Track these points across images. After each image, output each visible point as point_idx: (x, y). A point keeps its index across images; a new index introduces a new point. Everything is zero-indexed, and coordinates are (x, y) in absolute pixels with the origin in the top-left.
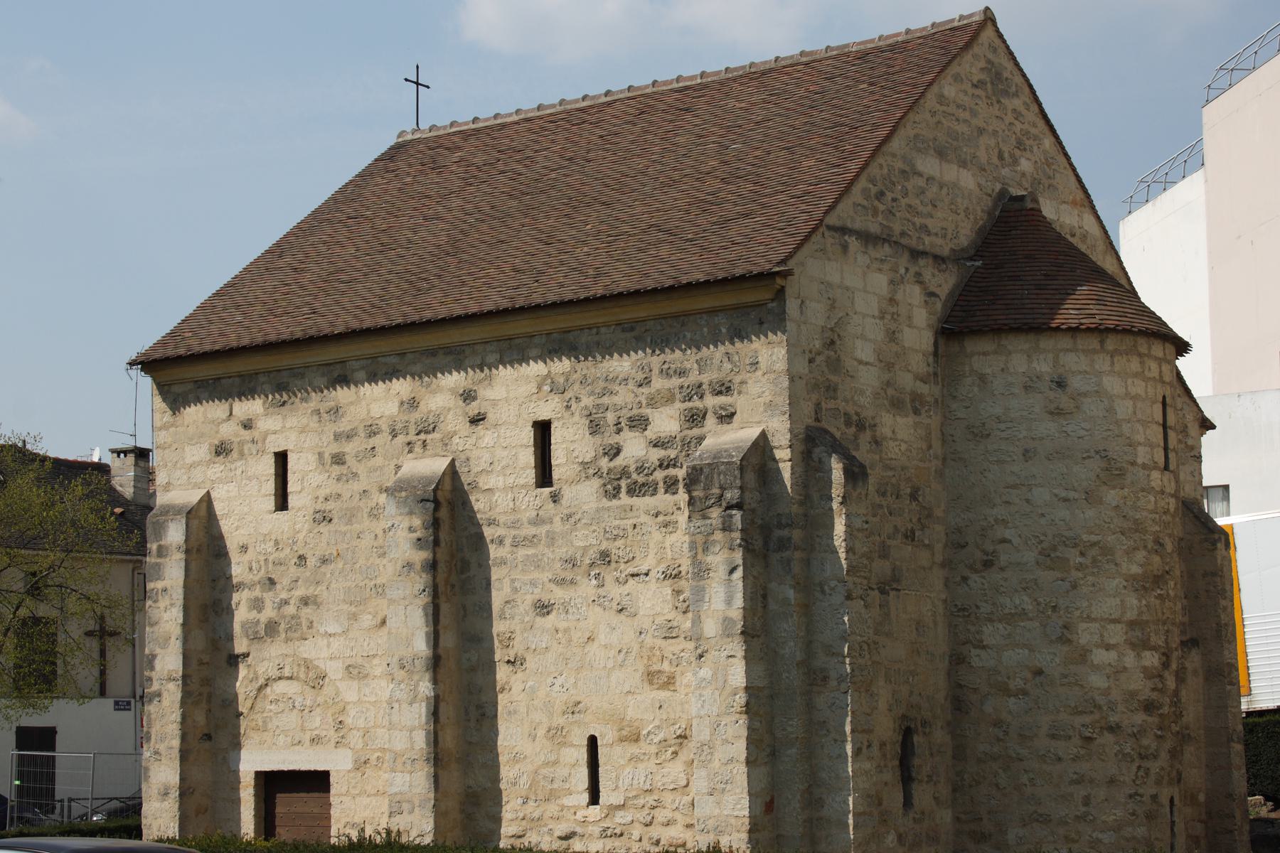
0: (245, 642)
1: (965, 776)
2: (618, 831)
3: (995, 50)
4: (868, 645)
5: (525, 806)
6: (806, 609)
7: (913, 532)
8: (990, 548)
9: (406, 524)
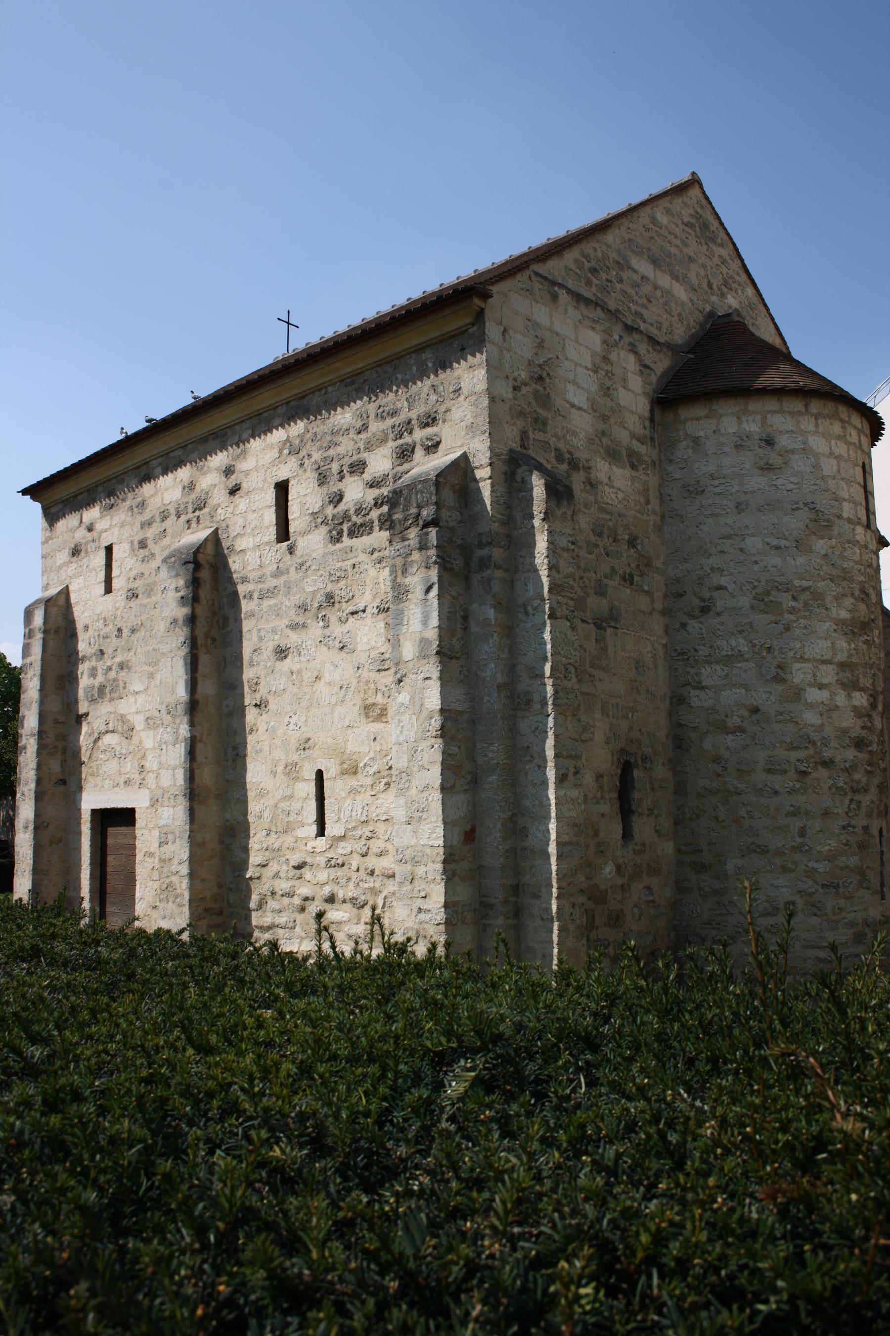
0: (86, 703)
1: (687, 810)
2: (340, 861)
3: (702, 207)
4: (576, 668)
5: (269, 838)
6: (510, 631)
7: (631, 576)
8: (707, 595)
9: (173, 586)
